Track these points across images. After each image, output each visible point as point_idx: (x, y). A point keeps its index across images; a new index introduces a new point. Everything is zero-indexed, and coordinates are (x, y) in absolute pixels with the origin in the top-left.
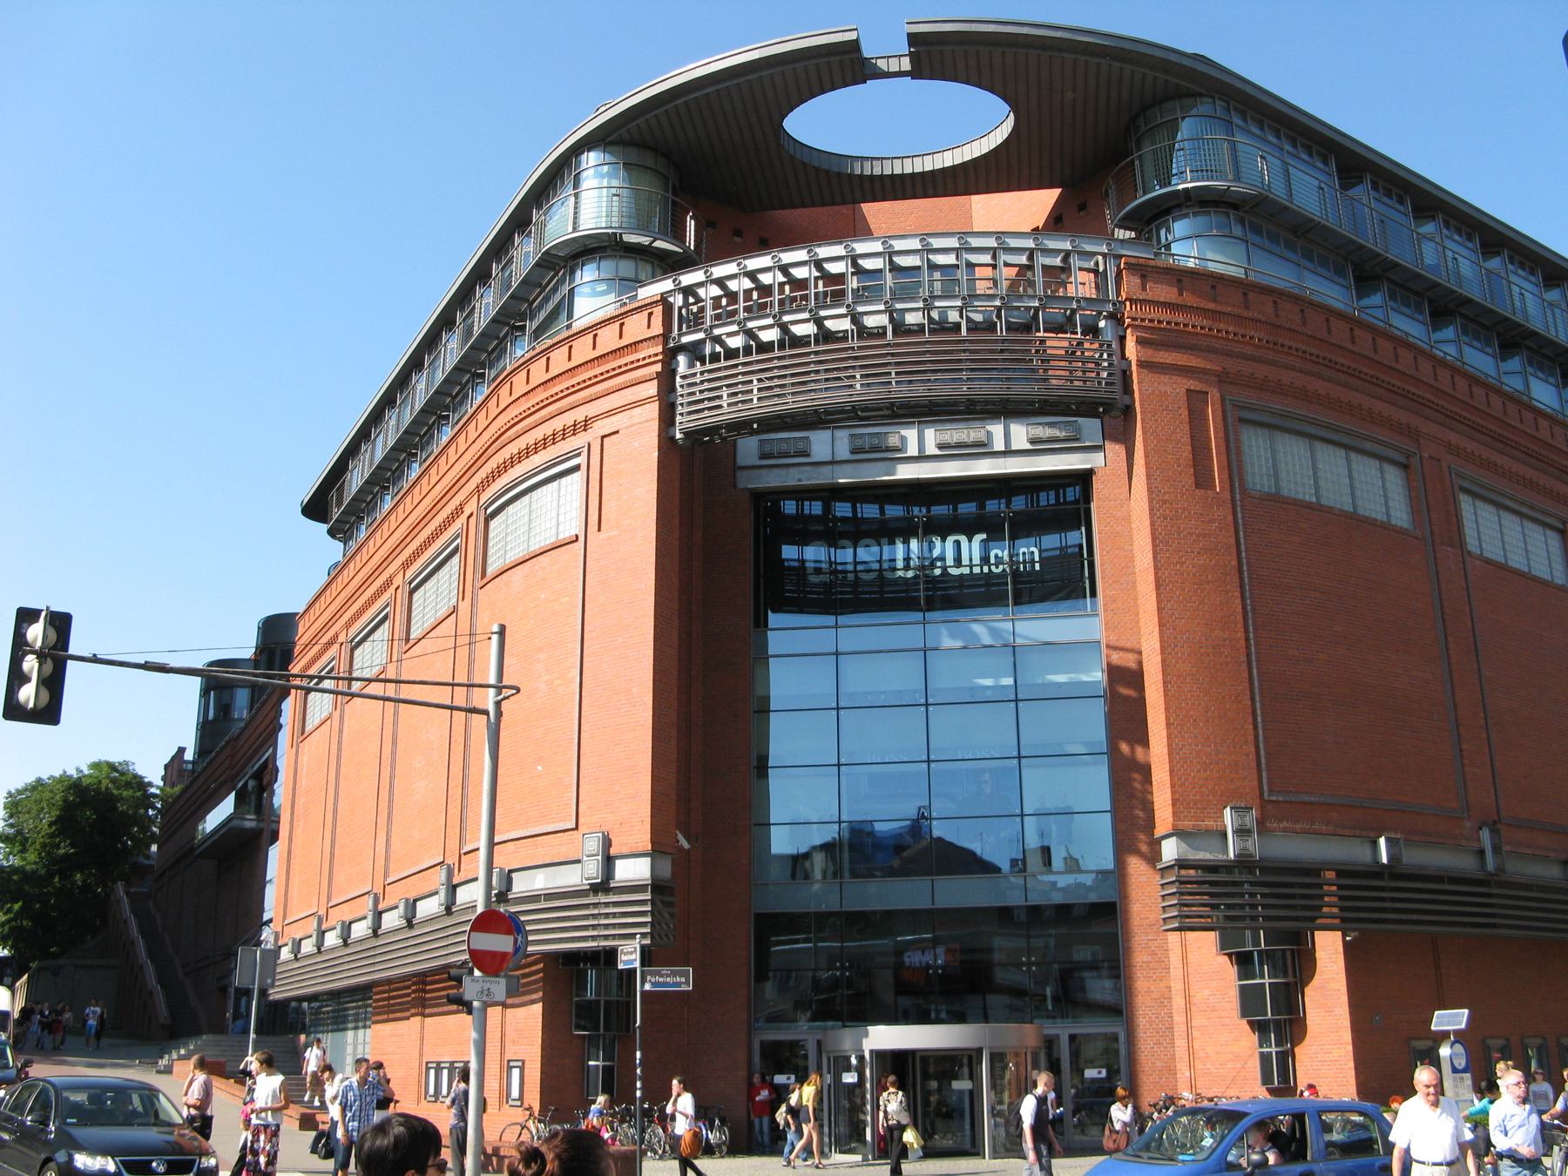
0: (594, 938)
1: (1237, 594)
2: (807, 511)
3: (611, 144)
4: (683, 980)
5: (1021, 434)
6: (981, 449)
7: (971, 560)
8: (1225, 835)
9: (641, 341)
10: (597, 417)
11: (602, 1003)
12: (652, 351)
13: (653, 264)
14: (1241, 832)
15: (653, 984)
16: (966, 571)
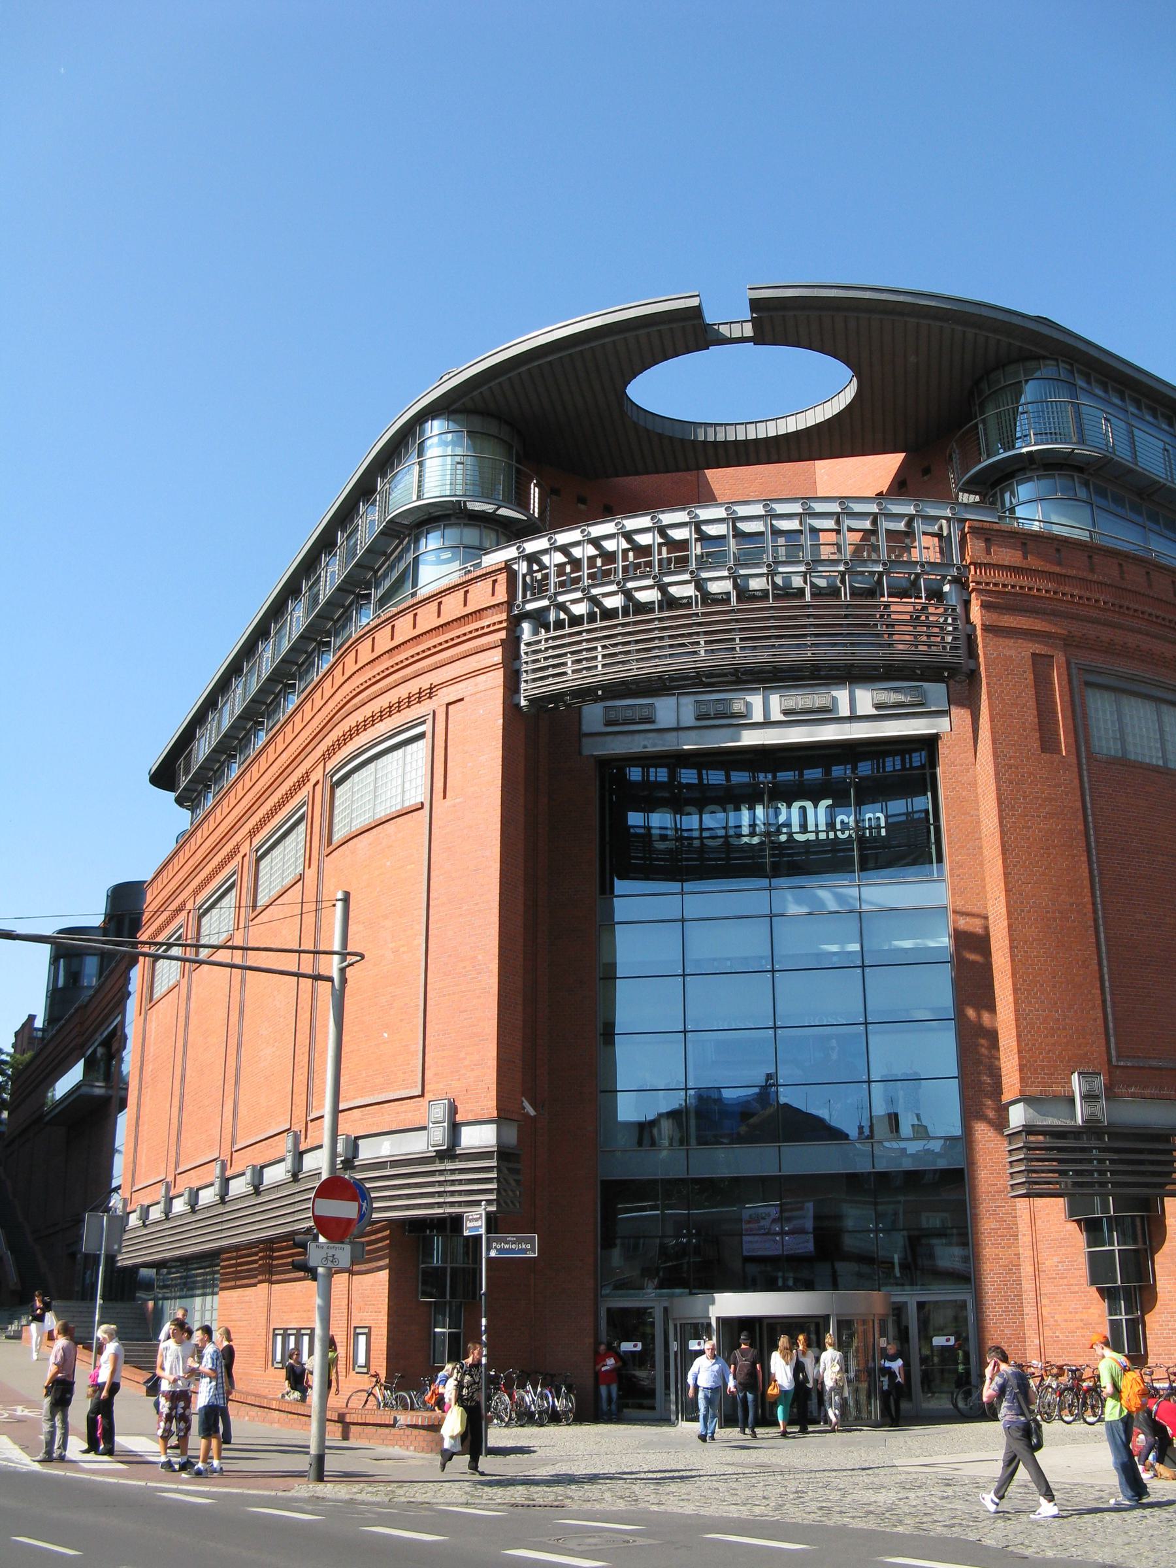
0: (440, 1205)
1: (1084, 858)
2: (652, 778)
3: (455, 412)
4: (529, 1246)
5: (866, 699)
6: (827, 715)
7: (817, 826)
8: (1072, 1101)
9: (486, 609)
11: (449, 1270)
12: (496, 618)
13: (497, 531)
14: (1089, 1097)
15: (499, 1251)
16: (812, 837)
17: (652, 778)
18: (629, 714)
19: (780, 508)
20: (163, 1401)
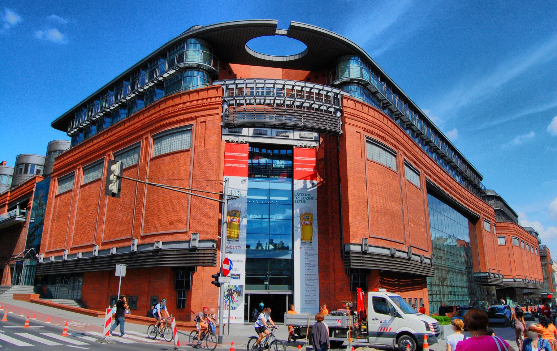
1: (365, 184)
2: (255, 151)
3: (198, 38)
10: (199, 117)
17: (255, 151)
18: (260, 132)
19: (267, 81)
20: (442, 296)
